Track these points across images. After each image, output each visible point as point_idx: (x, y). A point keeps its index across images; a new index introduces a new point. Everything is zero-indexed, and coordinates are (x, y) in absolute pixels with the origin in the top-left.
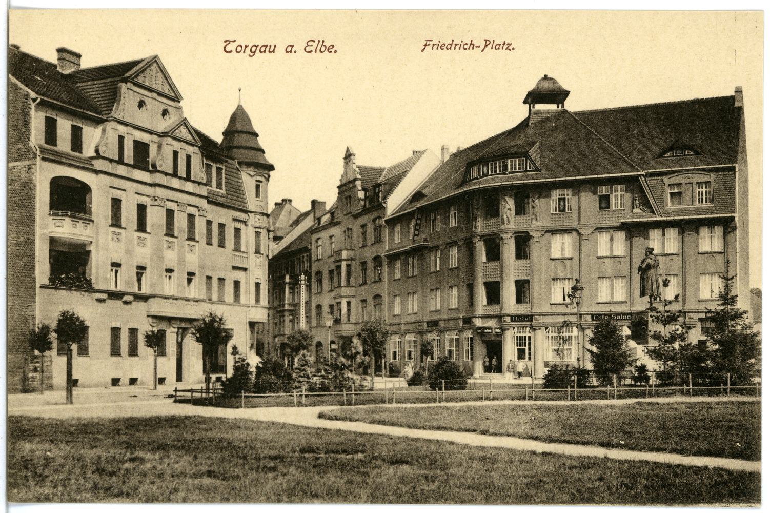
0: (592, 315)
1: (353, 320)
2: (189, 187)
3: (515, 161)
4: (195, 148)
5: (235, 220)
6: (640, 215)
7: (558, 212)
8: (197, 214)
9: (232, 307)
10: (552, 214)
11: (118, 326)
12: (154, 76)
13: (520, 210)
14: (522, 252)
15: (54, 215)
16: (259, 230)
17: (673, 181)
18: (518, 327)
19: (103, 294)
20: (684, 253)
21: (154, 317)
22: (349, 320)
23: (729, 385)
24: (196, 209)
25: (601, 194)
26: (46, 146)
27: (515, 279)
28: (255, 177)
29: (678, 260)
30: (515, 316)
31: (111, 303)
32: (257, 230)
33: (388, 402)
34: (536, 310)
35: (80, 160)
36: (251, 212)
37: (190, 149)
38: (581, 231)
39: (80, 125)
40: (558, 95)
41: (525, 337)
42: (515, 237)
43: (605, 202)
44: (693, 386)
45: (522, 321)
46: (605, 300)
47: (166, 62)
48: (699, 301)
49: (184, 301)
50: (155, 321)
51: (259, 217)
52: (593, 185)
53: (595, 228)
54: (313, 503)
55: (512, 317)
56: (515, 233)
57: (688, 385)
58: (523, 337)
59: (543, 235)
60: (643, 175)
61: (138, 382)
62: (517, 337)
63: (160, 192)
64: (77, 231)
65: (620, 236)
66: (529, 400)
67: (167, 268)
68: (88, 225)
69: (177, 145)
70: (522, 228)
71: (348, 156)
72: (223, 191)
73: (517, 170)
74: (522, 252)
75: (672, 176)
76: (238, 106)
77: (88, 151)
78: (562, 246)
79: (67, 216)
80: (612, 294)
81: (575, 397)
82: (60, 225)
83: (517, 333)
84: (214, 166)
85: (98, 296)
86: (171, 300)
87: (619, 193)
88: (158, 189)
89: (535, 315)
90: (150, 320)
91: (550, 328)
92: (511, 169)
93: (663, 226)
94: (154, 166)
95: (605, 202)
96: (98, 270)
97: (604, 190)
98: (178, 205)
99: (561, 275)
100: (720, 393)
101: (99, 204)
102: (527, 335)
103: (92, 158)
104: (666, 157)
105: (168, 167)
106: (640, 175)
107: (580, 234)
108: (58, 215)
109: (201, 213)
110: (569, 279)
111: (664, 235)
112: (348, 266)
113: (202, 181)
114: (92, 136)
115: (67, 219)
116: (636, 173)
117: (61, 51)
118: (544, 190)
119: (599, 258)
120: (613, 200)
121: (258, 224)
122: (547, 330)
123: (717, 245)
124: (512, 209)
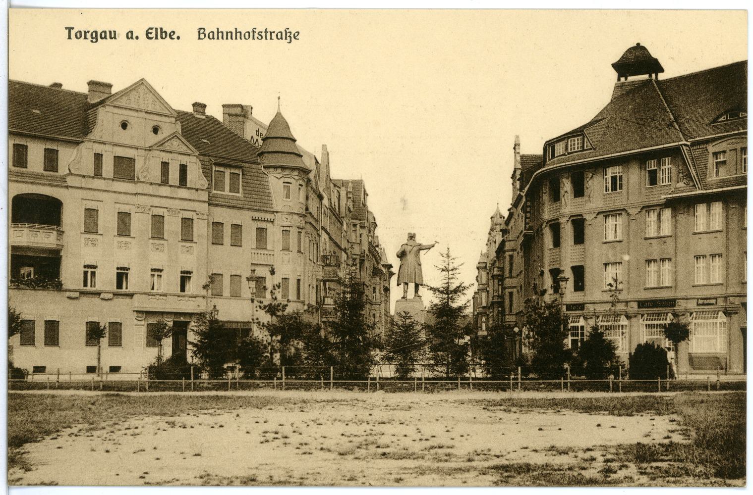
1: (514, 311)
6: (682, 189)
7: (610, 191)
8: (195, 217)
9: (228, 300)
10: (604, 195)
11: (118, 320)
12: (142, 97)
13: (579, 192)
14: (579, 238)
15: (14, 227)
16: (288, 229)
17: (718, 148)
18: (648, 314)
19: (76, 293)
22: (511, 311)
23: (332, 379)
25: (650, 169)
26: (13, 169)
27: (571, 265)
28: (283, 178)
30: (570, 305)
31: (85, 300)
33: (417, 390)
34: (588, 298)
35: (55, 179)
36: (277, 212)
37: (184, 160)
38: (629, 211)
39: (55, 148)
41: (578, 326)
42: (572, 221)
43: (653, 179)
44: (333, 379)
45: (576, 310)
46: (653, 286)
47: (150, 80)
49: (176, 297)
50: (140, 315)
51: (287, 216)
52: (642, 159)
53: (642, 206)
55: (567, 305)
56: (572, 216)
57: (566, 378)
61: (122, 370)
63: (141, 200)
64: (36, 240)
65: (667, 213)
67: (183, 270)
68: (38, 233)
69: (166, 157)
70: (577, 211)
71: (516, 146)
72: (240, 195)
73: (576, 150)
74: (579, 238)
75: (724, 140)
76: (277, 113)
77: (63, 170)
78: (613, 228)
79: (25, 227)
80: (709, 277)
81: (147, 388)
83: (647, 320)
85: (68, 294)
86: (158, 296)
87: (667, 167)
90: (135, 313)
91: (695, 314)
92: (571, 149)
93: (708, 199)
95: (653, 179)
100: (320, 388)
101: (72, 216)
102: (580, 324)
104: (720, 122)
106: (681, 145)
107: (628, 214)
108: (18, 227)
109: (200, 216)
112: (511, 257)
114: (66, 156)
115: (25, 230)
116: (677, 144)
117: (91, 83)
118: (601, 166)
121: (285, 223)
123: (717, 223)
124: (569, 192)
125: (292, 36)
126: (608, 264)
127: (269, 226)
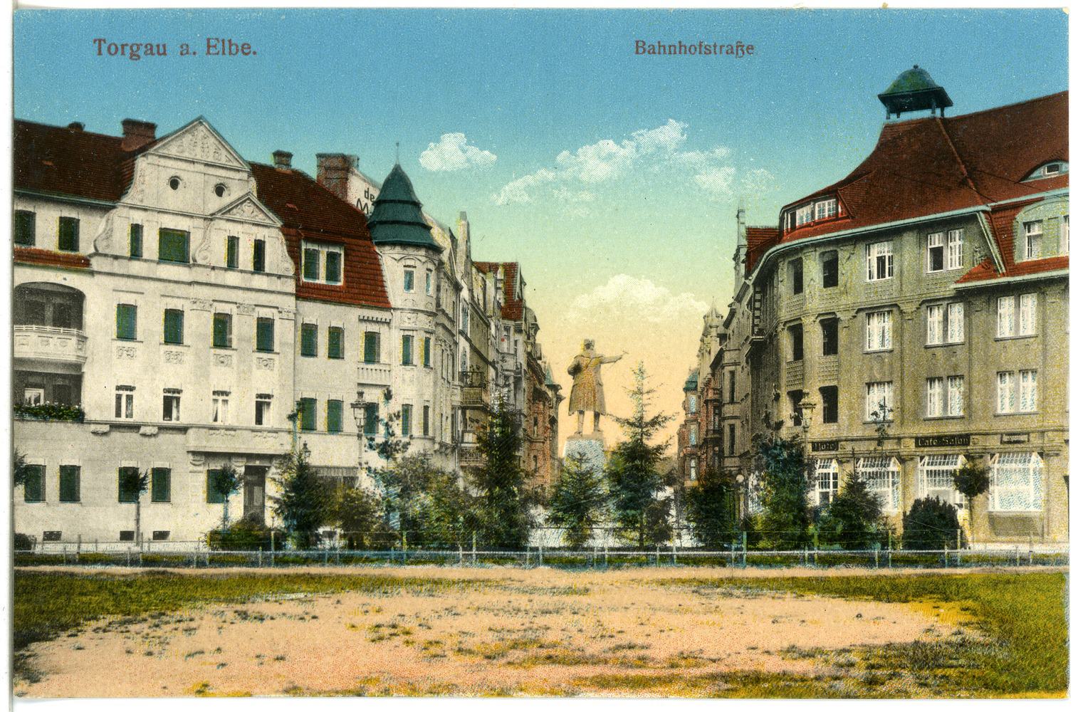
0: (917, 439)
2: (259, 281)
3: (824, 205)
4: (272, 230)
5: (362, 320)
20: (1045, 334)
21: (194, 453)
24: (275, 311)
25: (933, 246)
29: (1036, 346)
30: (818, 443)
32: (407, 333)
36: (394, 309)
37: (261, 233)
40: (939, 98)
41: (829, 474)
42: (821, 322)
48: (995, 416)
50: (198, 458)
51: (409, 315)
54: (986, 697)
58: (935, 471)
59: (854, 317)
60: (984, 212)
61: (171, 536)
62: (927, 471)
66: (1021, 565)
77: (85, 248)
79: (32, 331)
82: (25, 342)
83: (928, 464)
84: (323, 253)
85: (93, 427)
86: (265, 433)
88: (197, 287)
89: (972, 434)
90: (191, 457)
91: (997, 455)
94: (195, 260)
96: (96, 398)
97: (936, 240)
98: (238, 307)
99: (878, 377)
101: (99, 312)
103: (91, 256)
105: (221, 258)
106: (978, 212)
110: (888, 383)
111: (1018, 306)
113: (286, 274)
114: (91, 228)
119: (927, 348)
120: (947, 255)
121: (406, 325)
122: (993, 460)
125: (745, 48)
126: (873, 384)
127: (383, 330)
